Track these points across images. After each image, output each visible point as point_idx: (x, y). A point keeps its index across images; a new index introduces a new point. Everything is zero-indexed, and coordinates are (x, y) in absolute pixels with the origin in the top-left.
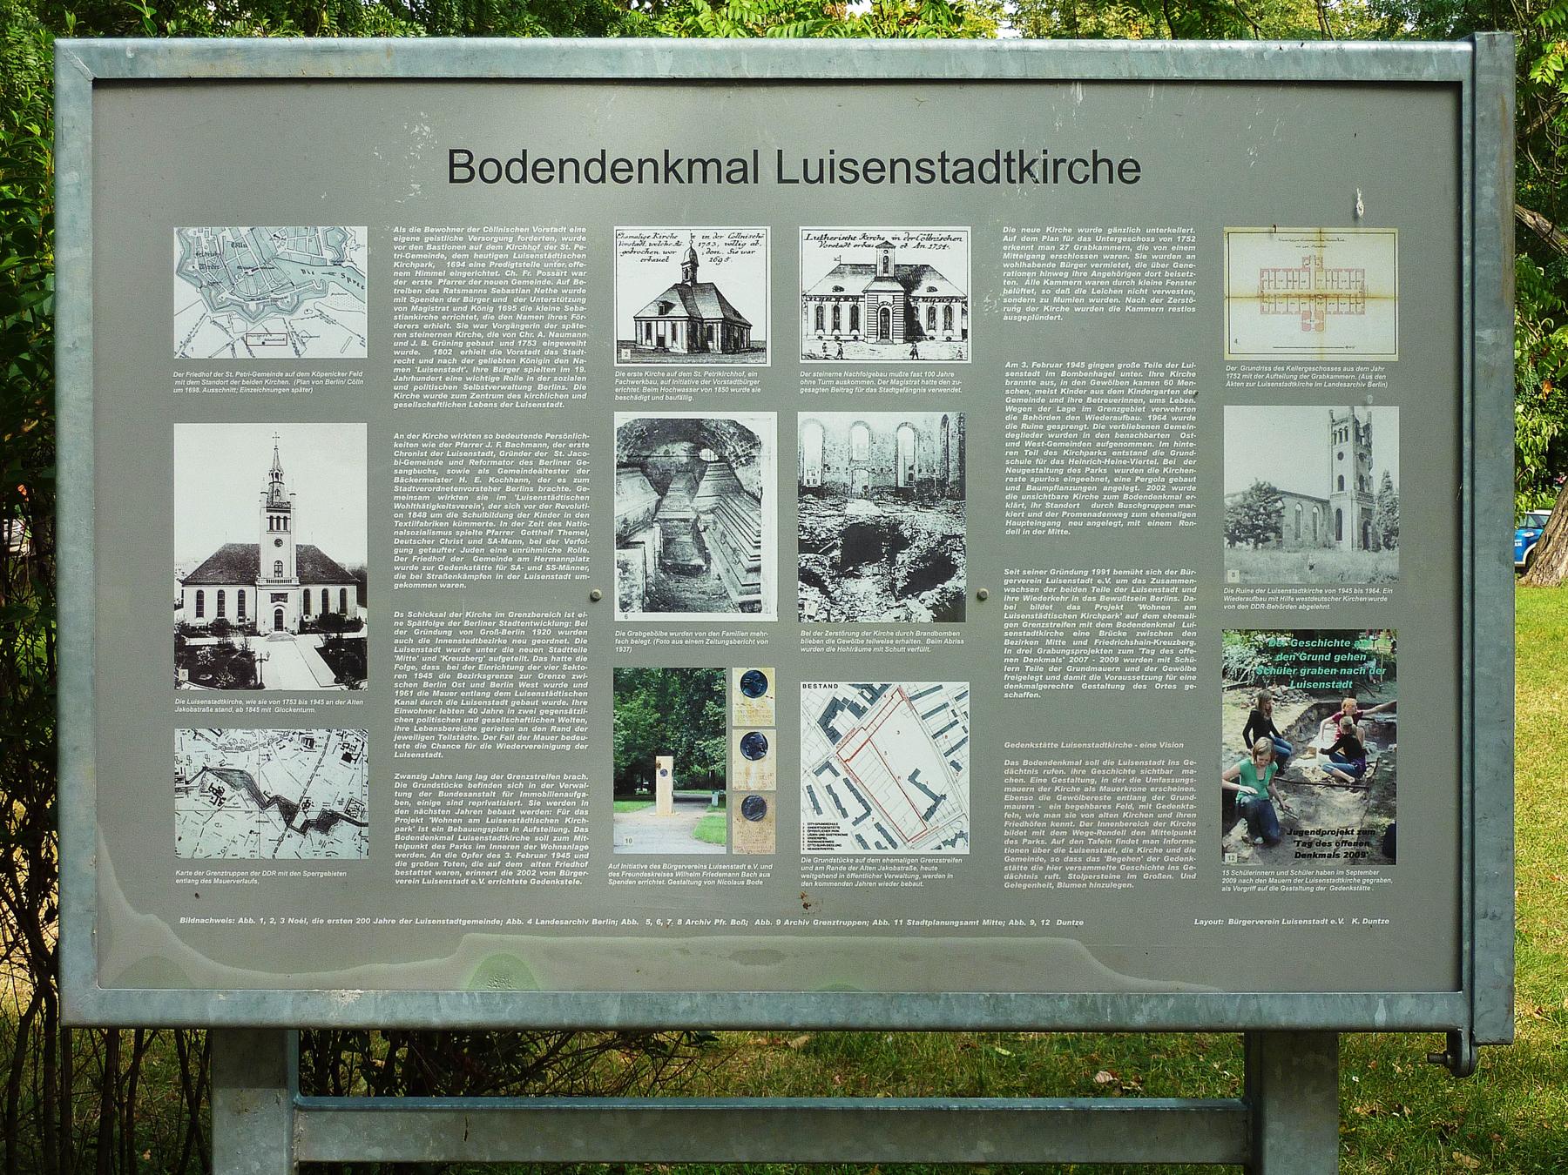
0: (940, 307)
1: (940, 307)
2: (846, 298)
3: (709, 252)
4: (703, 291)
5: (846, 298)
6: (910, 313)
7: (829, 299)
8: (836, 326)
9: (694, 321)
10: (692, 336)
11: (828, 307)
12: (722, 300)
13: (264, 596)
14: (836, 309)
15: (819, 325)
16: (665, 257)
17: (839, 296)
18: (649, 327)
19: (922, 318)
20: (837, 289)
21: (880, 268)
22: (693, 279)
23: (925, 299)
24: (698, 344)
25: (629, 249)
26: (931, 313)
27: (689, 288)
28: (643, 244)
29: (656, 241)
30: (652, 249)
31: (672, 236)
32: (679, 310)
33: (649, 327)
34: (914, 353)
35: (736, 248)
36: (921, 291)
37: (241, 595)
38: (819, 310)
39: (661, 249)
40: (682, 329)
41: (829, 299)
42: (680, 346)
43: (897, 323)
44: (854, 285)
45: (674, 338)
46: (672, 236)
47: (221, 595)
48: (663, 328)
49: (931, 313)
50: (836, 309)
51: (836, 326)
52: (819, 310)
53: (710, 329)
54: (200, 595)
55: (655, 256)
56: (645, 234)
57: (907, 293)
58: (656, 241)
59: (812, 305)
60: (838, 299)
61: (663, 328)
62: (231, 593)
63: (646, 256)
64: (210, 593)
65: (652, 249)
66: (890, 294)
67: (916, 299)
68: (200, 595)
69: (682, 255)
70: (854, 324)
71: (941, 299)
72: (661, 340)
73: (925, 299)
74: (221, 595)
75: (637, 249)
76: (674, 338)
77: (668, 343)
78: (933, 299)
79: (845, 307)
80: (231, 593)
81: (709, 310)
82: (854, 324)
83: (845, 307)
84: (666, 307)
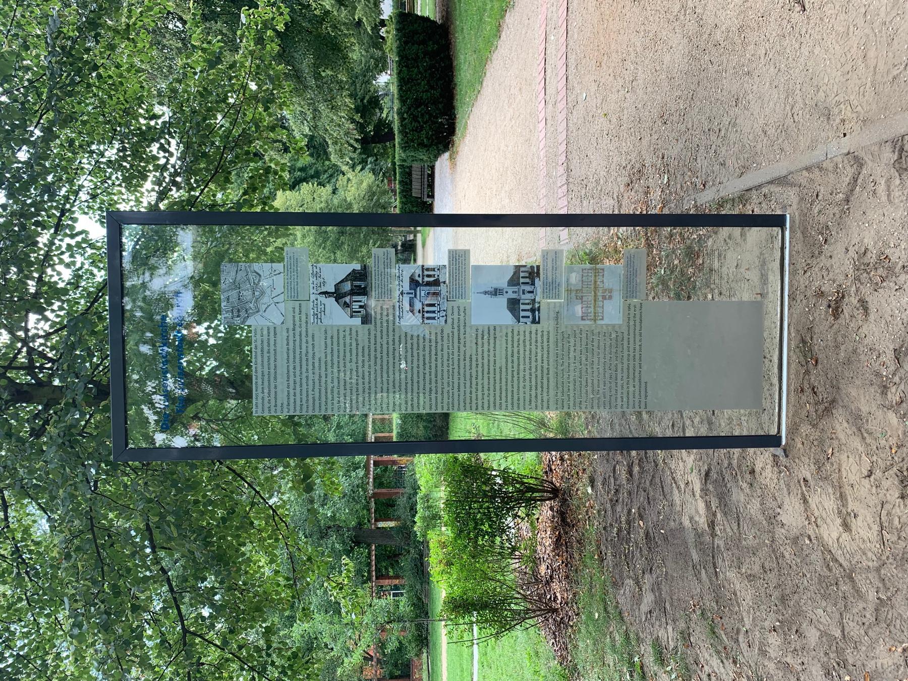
0: (426, 273)
1: (426, 273)
2: (423, 308)
3: (320, 286)
4: (338, 289)
5: (423, 308)
6: (428, 284)
7: (423, 315)
8: (434, 312)
9: (352, 293)
10: (359, 294)
11: (426, 315)
12: (342, 281)
13: (523, 297)
14: (427, 312)
15: (434, 318)
16: (323, 306)
17: (422, 311)
18: (355, 312)
19: (431, 279)
20: (419, 312)
21: (411, 296)
22: (333, 293)
23: (423, 279)
24: (363, 292)
25: (319, 321)
26: (429, 276)
27: (338, 295)
28: (317, 314)
29: (315, 309)
30: (319, 310)
31: (313, 302)
32: (347, 299)
33: (355, 312)
34: (444, 282)
35: (318, 275)
36: (420, 280)
37: (523, 304)
38: (428, 318)
39: (319, 307)
40: (355, 298)
41: (423, 315)
42: (363, 299)
43: (433, 289)
44: (418, 306)
45: (360, 301)
46: (313, 302)
47: (522, 310)
48: (356, 306)
49: (429, 276)
50: (427, 312)
51: (434, 312)
52: (428, 318)
53: (355, 286)
54: (523, 317)
55: (323, 309)
56: (312, 313)
57: (422, 285)
58: (315, 309)
59: (426, 321)
60: (423, 312)
61: (356, 306)
62: (522, 307)
63: (323, 313)
64: (522, 314)
65: (319, 310)
66: (422, 291)
67: (423, 282)
68: (523, 317)
69: (322, 298)
70: (433, 305)
71: (423, 272)
72: (361, 307)
73: (423, 279)
74: (522, 310)
75: (319, 317)
76: (360, 301)
77: (362, 304)
78: (423, 276)
79: (426, 309)
80: (522, 307)
81: (347, 286)
82: (433, 305)
83: (426, 309)
84: (346, 305)
